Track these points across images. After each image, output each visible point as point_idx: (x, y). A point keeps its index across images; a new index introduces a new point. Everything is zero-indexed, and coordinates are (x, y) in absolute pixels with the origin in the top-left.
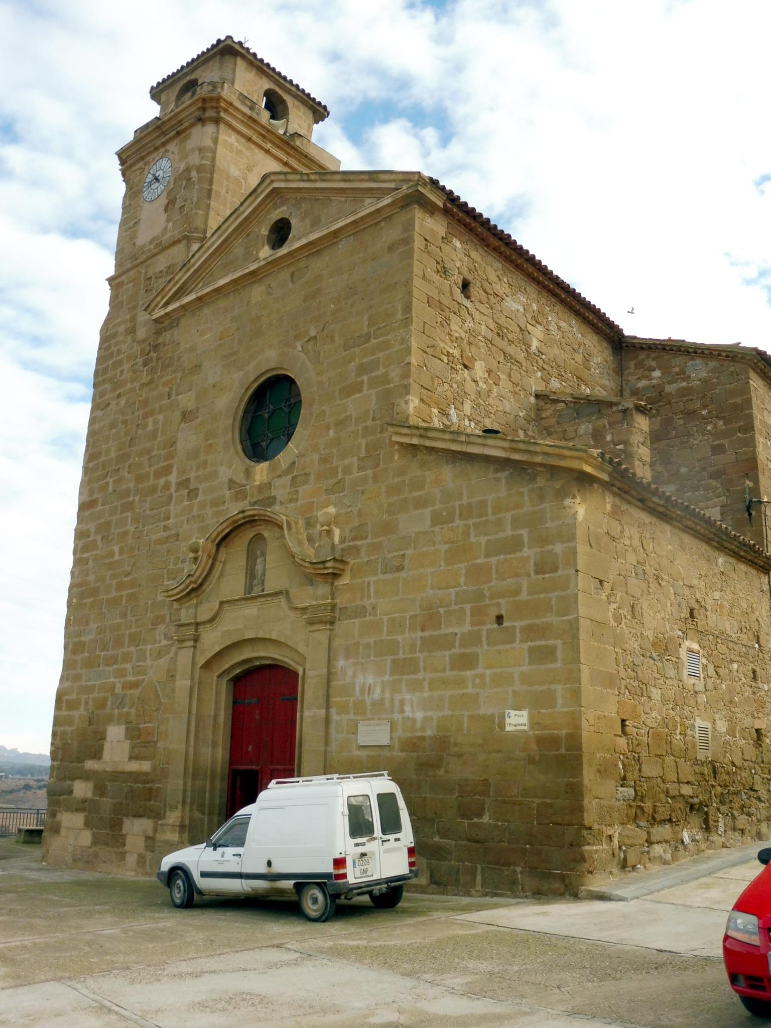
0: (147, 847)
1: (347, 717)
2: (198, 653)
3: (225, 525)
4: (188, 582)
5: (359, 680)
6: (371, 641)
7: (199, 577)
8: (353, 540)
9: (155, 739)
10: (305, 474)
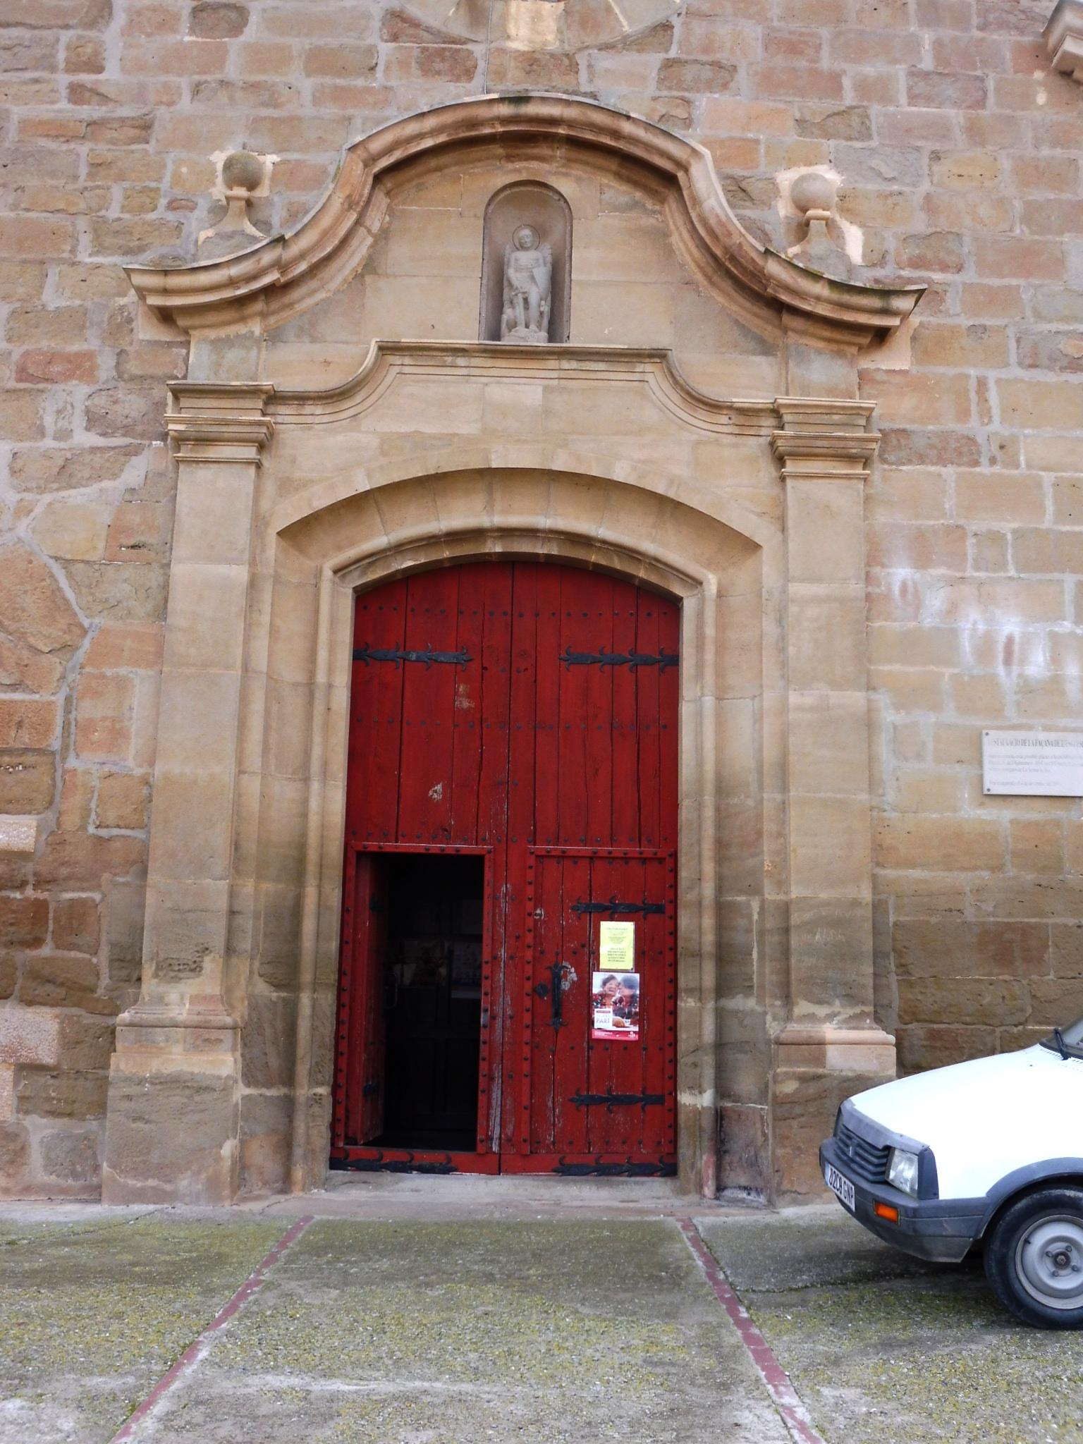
0: (22, 1099)
1: (932, 718)
2: (270, 487)
3: (431, 122)
4: (267, 258)
5: (972, 622)
6: (1007, 526)
7: (302, 256)
8: (917, 263)
9: (56, 744)
10: (717, 65)
